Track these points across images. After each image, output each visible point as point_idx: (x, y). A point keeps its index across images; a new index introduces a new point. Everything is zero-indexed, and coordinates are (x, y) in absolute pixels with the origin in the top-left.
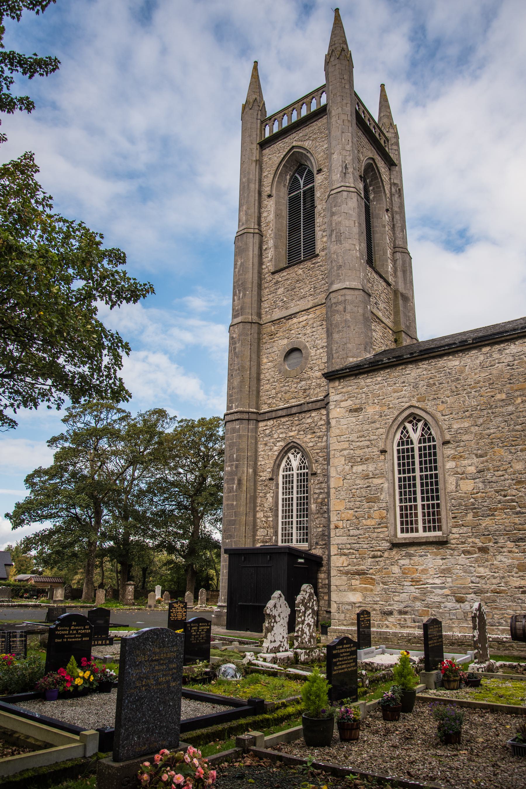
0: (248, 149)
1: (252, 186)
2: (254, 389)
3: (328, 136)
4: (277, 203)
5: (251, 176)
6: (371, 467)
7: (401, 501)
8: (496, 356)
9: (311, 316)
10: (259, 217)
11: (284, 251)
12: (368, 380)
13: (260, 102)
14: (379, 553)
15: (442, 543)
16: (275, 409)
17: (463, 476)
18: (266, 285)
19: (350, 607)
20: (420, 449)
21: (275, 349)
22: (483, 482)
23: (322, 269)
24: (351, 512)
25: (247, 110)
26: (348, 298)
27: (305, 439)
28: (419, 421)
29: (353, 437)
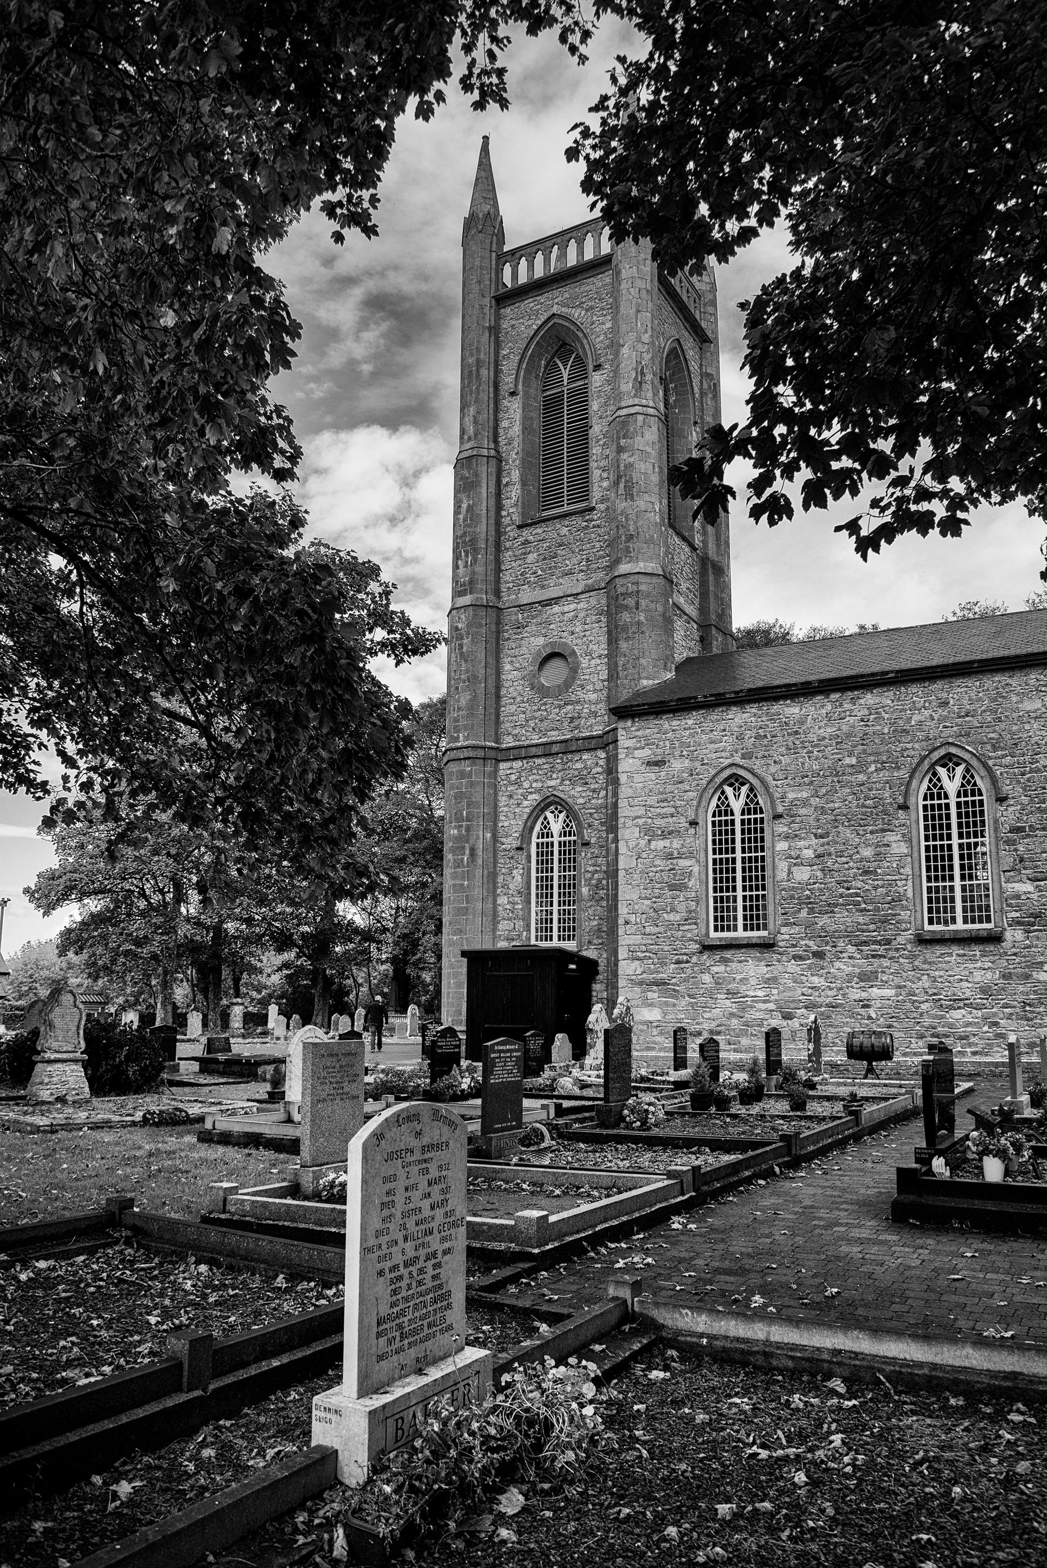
0: (477, 306)
1: (484, 372)
2: (492, 711)
4: (525, 407)
6: (676, 844)
7: (715, 890)
8: (847, 706)
9: (582, 605)
12: (675, 723)
13: (495, 219)
14: (685, 958)
15: (767, 946)
16: (526, 743)
17: (797, 861)
18: (508, 544)
21: (524, 650)
24: (647, 902)
26: (642, 587)
27: (572, 792)
28: (743, 784)
29: (652, 801)
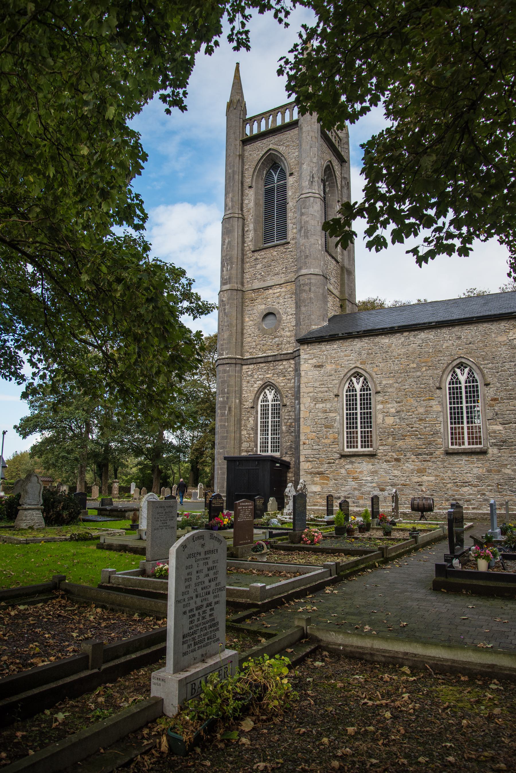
1: (236, 177)
3: (300, 146)
4: (256, 194)
5: (235, 169)
6: (328, 406)
7: (347, 428)
9: (283, 290)
10: (242, 204)
11: (261, 233)
12: (328, 347)
15: (372, 455)
16: (256, 356)
17: (387, 414)
18: (248, 260)
19: (313, 495)
20: (361, 395)
21: (255, 311)
22: (399, 419)
23: (293, 254)
25: (231, 109)
26: (313, 281)
27: (278, 380)
28: (361, 377)
29: (317, 384)
